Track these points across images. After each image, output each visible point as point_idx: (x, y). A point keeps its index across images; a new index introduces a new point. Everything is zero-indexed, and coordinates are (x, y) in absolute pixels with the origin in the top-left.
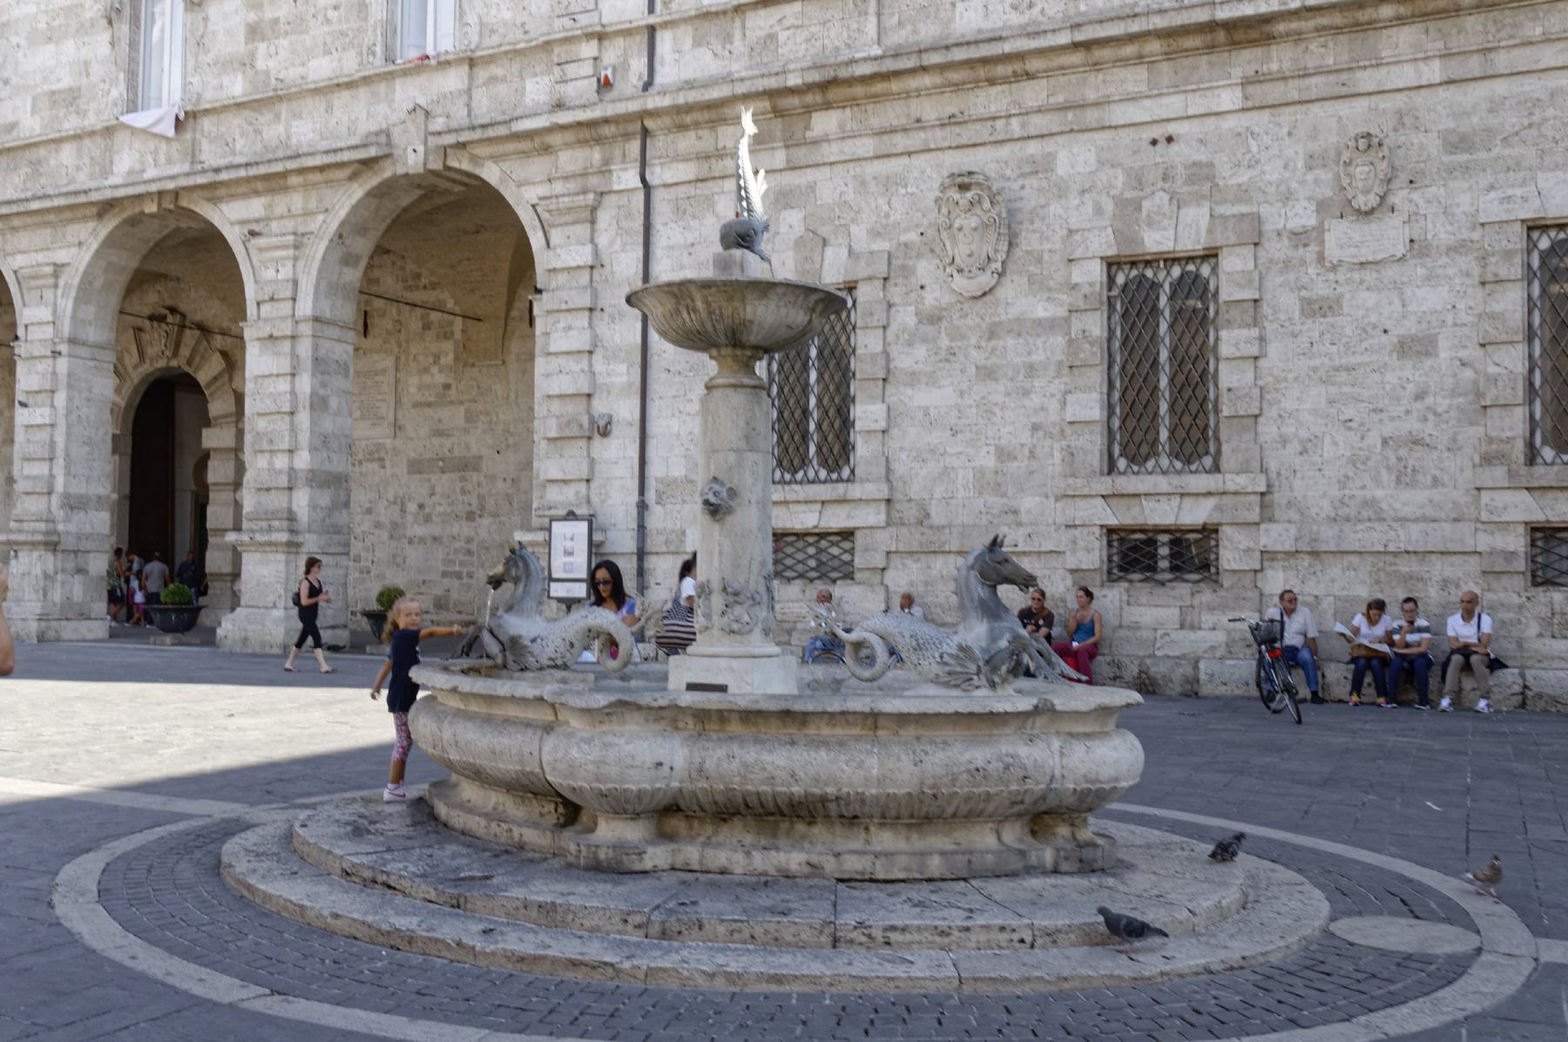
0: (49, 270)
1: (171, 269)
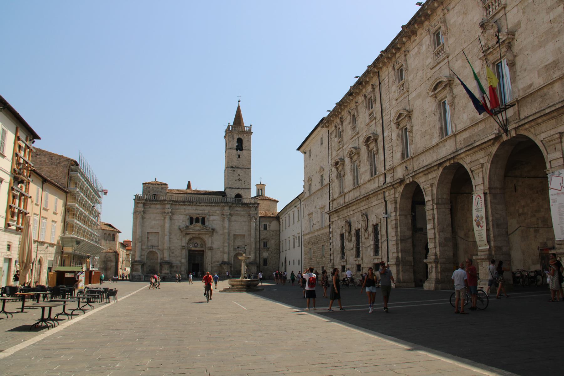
0: (558, 136)
1: (414, 197)
